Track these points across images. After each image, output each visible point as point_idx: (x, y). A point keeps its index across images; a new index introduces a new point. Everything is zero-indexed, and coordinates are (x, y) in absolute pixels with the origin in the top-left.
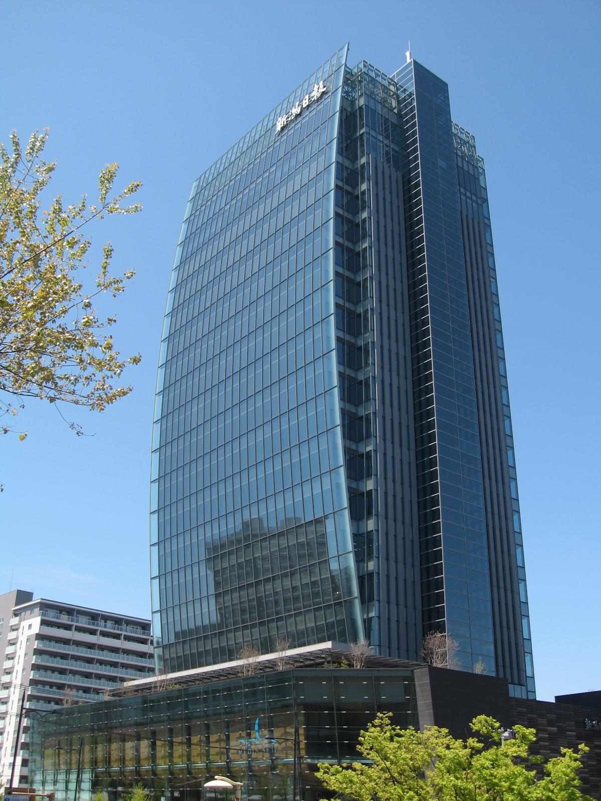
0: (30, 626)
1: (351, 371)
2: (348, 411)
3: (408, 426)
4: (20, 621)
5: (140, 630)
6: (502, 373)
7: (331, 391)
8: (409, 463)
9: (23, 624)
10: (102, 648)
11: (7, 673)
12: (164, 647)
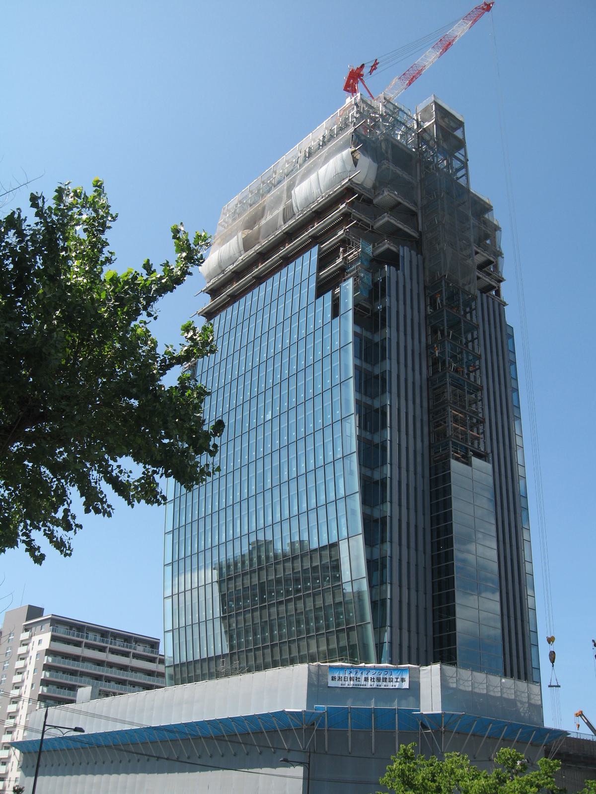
0: (40, 642)
1: (368, 399)
2: (365, 403)
3: (424, 529)
4: (31, 637)
5: (148, 648)
6: (515, 404)
7: (347, 381)
8: (425, 568)
9: (34, 638)
10: (111, 665)
11: (10, 717)
12: (175, 666)
